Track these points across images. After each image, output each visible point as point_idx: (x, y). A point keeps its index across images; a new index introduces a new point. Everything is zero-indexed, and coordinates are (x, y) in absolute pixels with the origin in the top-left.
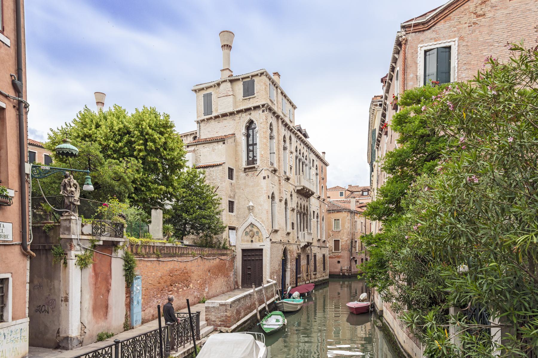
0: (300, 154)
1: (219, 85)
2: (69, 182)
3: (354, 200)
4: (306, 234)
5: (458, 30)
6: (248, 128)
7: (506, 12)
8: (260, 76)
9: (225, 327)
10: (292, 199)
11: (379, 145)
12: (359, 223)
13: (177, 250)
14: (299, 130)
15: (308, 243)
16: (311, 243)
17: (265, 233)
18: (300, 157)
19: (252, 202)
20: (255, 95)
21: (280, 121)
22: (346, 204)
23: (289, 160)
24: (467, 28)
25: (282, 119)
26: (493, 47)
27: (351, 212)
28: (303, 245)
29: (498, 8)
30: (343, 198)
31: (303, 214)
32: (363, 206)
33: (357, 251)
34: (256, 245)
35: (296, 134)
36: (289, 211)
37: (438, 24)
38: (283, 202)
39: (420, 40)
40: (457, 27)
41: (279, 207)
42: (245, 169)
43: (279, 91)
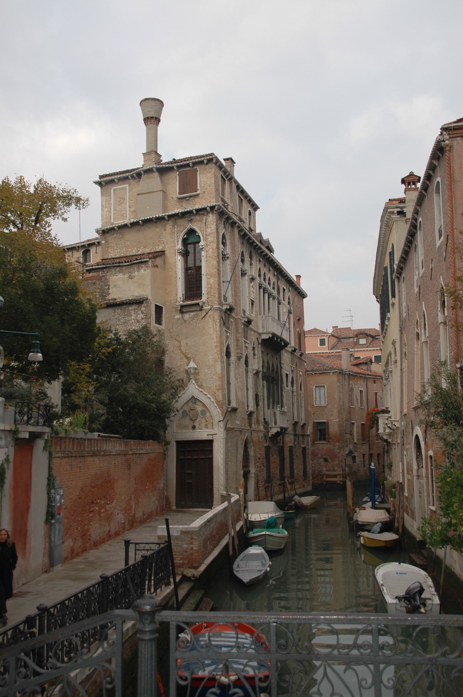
0: (265, 279)
1: (139, 175)
4: (278, 413)
8: (207, 164)
11: (400, 274)
12: (356, 392)
15: (282, 428)
16: (286, 429)
17: (216, 413)
18: (266, 284)
19: (194, 361)
20: (199, 192)
21: (236, 230)
23: (249, 290)
27: (341, 373)
28: (273, 431)
30: (325, 350)
31: (272, 378)
32: (361, 364)
33: (355, 441)
34: (202, 434)
35: (260, 248)
36: (250, 375)
41: (236, 371)
42: (182, 306)
43: (234, 186)
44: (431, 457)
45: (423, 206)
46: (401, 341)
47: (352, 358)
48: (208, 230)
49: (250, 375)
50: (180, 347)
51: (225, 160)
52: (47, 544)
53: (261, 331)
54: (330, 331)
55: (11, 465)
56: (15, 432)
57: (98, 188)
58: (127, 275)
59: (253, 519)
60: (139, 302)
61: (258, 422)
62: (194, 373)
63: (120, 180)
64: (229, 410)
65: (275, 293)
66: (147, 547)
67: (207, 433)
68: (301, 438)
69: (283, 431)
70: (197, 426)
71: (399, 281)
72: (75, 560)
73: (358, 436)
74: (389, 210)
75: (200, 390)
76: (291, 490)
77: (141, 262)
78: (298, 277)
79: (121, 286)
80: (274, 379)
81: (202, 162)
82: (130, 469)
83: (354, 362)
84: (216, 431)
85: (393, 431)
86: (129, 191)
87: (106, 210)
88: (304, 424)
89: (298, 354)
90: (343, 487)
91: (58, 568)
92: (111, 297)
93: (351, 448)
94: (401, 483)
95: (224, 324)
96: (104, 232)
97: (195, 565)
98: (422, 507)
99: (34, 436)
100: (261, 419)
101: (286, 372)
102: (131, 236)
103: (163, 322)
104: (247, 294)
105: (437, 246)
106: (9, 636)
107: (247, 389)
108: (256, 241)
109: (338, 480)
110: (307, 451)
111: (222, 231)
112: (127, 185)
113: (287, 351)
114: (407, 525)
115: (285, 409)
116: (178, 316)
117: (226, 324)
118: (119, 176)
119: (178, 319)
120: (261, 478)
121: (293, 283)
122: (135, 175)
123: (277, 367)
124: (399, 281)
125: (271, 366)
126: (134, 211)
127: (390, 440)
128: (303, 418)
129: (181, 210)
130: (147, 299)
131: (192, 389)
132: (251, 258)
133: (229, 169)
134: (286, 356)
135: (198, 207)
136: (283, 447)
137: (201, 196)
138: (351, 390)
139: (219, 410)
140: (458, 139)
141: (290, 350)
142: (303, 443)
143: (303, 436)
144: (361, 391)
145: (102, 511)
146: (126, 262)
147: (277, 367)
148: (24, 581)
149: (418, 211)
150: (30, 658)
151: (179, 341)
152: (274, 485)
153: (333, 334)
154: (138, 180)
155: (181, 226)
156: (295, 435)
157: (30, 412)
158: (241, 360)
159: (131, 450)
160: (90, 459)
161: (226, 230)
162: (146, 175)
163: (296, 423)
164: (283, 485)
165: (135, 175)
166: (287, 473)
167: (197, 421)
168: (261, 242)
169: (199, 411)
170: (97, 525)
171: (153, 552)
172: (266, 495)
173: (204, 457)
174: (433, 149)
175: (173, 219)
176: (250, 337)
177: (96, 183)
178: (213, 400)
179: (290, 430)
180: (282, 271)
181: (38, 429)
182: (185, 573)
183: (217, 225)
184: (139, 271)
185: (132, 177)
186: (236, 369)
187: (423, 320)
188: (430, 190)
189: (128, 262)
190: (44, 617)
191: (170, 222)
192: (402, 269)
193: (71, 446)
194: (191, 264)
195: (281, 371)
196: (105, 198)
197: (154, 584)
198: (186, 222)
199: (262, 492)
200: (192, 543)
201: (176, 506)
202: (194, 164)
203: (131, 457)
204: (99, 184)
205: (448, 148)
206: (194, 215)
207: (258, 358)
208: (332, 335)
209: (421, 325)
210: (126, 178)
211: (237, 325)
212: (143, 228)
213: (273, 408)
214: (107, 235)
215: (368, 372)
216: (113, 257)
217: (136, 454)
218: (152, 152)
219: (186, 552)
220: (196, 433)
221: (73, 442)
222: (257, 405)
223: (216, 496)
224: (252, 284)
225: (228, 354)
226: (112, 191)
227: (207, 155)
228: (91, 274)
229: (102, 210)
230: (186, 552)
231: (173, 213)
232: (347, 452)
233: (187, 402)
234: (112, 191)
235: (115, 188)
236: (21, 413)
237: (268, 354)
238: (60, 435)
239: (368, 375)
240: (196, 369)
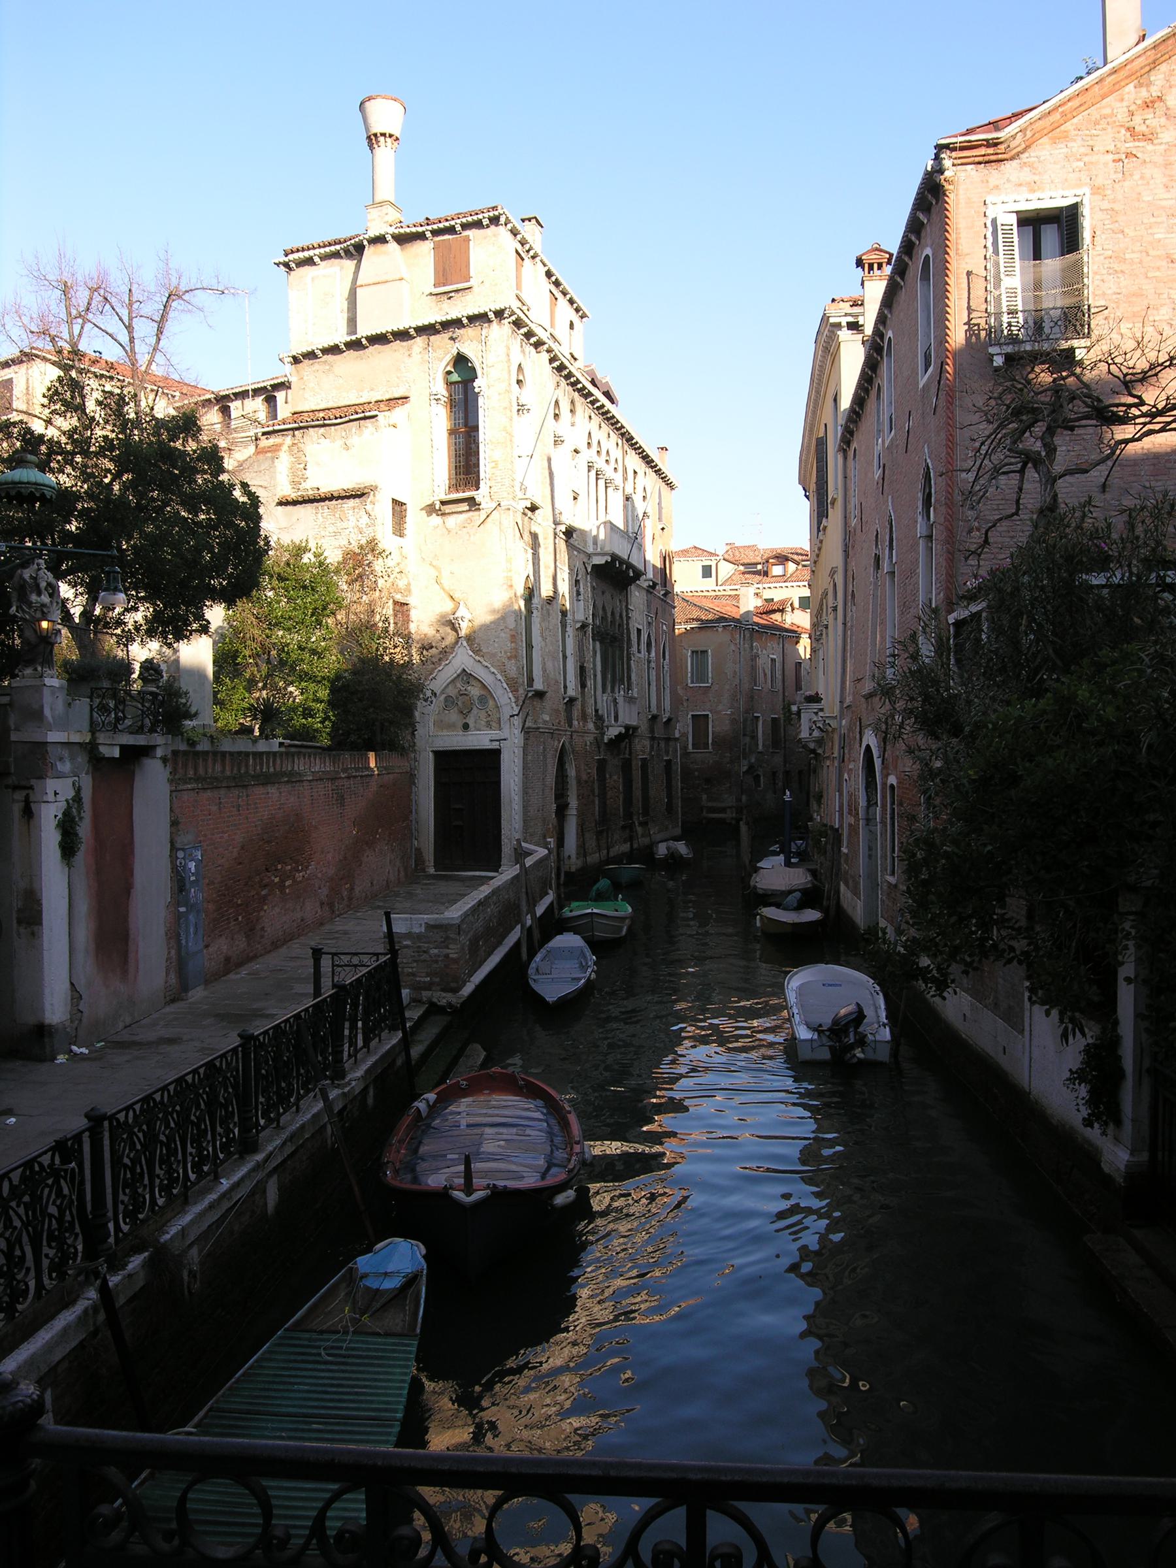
2: (35, 579)
4: (620, 700)
9: (443, 990)
13: (278, 761)
15: (627, 728)
16: (635, 728)
17: (506, 700)
18: (600, 463)
21: (545, 357)
24: (1112, 165)
28: (613, 732)
34: (479, 739)
35: (590, 394)
36: (570, 631)
40: (1086, 159)
44: (892, 786)
46: (846, 571)
52: (173, 952)
53: (590, 550)
54: (721, 550)
55: (87, 814)
56: (91, 749)
61: (584, 717)
63: (324, 258)
65: (618, 478)
67: (489, 737)
69: (629, 733)
70: (471, 725)
72: (232, 976)
73: (764, 741)
76: (643, 836)
80: (614, 639)
81: (478, 224)
84: (505, 733)
85: (826, 730)
88: (669, 720)
90: (737, 830)
91: (197, 994)
93: (753, 760)
94: (837, 830)
97: (453, 985)
98: (873, 888)
99: (134, 755)
100: (590, 710)
105: (921, 386)
106: (16, 1182)
107: (565, 657)
109: (729, 815)
110: (674, 768)
114: (845, 904)
115: (635, 692)
122: (351, 248)
125: (609, 615)
127: (820, 751)
128: (668, 708)
134: (637, 597)
138: (754, 658)
139: (511, 695)
141: (645, 585)
142: (667, 753)
143: (668, 740)
144: (773, 660)
145: (287, 883)
147: (621, 616)
148: (128, 1020)
149: (886, 317)
150: (493, 878)
153: (726, 556)
156: (653, 738)
157: (121, 707)
159: (345, 770)
160: (260, 790)
163: (654, 718)
164: (630, 827)
165: (351, 248)
167: (471, 715)
168: (593, 382)
169: (476, 698)
170: (277, 910)
171: (365, 970)
174: (920, 188)
178: (499, 677)
179: (644, 729)
181: (141, 740)
182: (435, 1000)
186: (543, 620)
187: (888, 530)
188: (910, 274)
190: (102, 1133)
193: (218, 767)
195: (628, 624)
197: (363, 1029)
203: (346, 783)
209: (883, 542)
213: (613, 691)
217: (355, 777)
221: (223, 761)
222: (583, 685)
223: (507, 849)
230: (437, 962)
232: (745, 769)
236: (104, 709)
238: (199, 748)
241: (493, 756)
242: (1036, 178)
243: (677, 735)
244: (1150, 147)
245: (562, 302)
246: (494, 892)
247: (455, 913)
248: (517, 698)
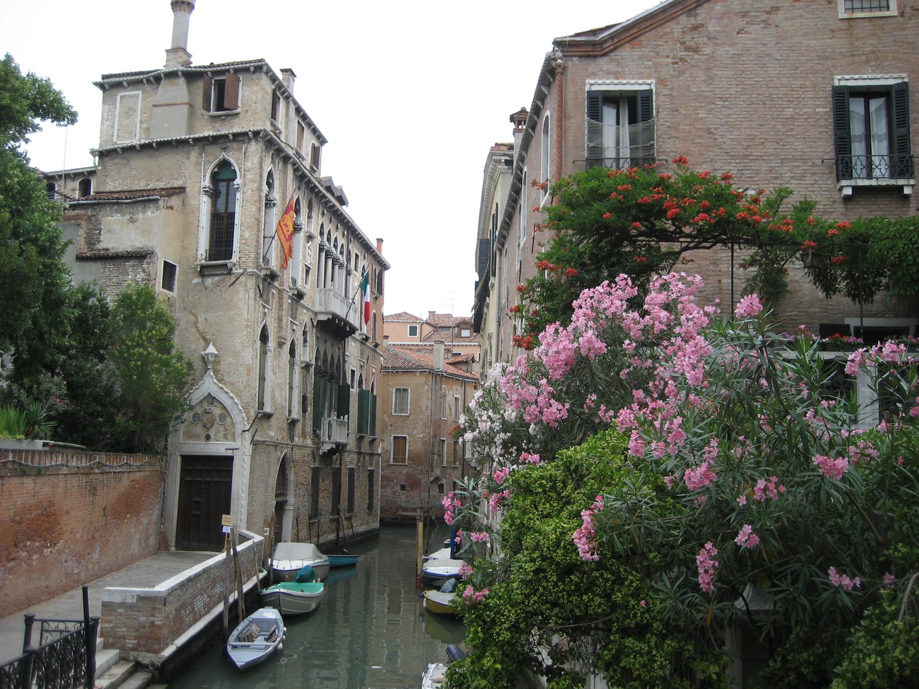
0: (329, 240)
3: (442, 347)
5: (656, 65)
6: (215, 178)
7: (732, 50)
8: (254, 72)
9: (148, 651)
10: (305, 341)
11: (503, 245)
12: (450, 399)
13: (37, 458)
14: (329, 189)
15: (338, 444)
16: (344, 445)
17: (241, 420)
19: (214, 345)
20: (239, 110)
21: (290, 169)
22: (422, 354)
23: (304, 253)
24: (671, 65)
25: (294, 164)
26: (714, 106)
28: (326, 447)
29: (719, 42)
30: (415, 341)
33: (445, 464)
34: (218, 448)
35: (324, 196)
36: (297, 369)
37: (621, 49)
38: (287, 348)
39: (589, 72)
41: (277, 363)
42: (203, 267)
43: (292, 108)
45: (530, 150)
47: (450, 355)
48: (250, 164)
49: (297, 369)
50: (195, 324)
51: (282, 71)
53: (317, 309)
57: (99, 93)
58: (127, 217)
59: (280, 568)
60: (140, 256)
61: (304, 435)
62: (214, 361)
64: (260, 415)
66: (62, 626)
67: (226, 447)
68: (367, 458)
71: (501, 255)
74: (494, 158)
75: (221, 385)
77: (149, 201)
78: (380, 241)
79: (119, 232)
80: (332, 377)
82: (94, 494)
83: (452, 360)
86: (143, 99)
87: (108, 123)
89: (370, 344)
92: (101, 246)
95: (261, 296)
96: (103, 154)
101: (352, 368)
102: (139, 163)
103: (176, 287)
104: (301, 258)
107: (291, 388)
108: (318, 185)
110: (375, 476)
111: (268, 167)
112: (140, 92)
113: (354, 338)
116: (197, 280)
117: (265, 297)
118: (129, 78)
119: (197, 284)
120: (303, 510)
121: (371, 248)
123: (339, 360)
124: (501, 255)
125: (329, 358)
126: (148, 129)
129: (212, 133)
130: (152, 253)
131: (209, 385)
132: (310, 208)
133: (285, 84)
134: (352, 347)
135: (236, 130)
136: (340, 469)
137: (241, 116)
139: (244, 415)
140: (575, 59)
141: (359, 338)
142: (371, 464)
143: (372, 455)
146: (127, 199)
147: (339, 360)
151: (195, 316)
152: (323, 520)
153: (429, 321)
154: (156, 86)
155: (211, 154)
156: (359, 453)
158: (284, 347)
160: (16, 481)
161: (274, 165)
162: (167, 81)
166: (344, 503)
170: (23, 579)
172: (310, 534)
173: (218, 480)
175: (201, 144)
176: (300, 317)
177: (96, 84)
180: (355, 230)
182: (140, 659)
183: (261, 158)
184: (144, 213)
185: (148, 81)
186: (275, 359)
189: (130, 198)
191: (196, 148)
192: (505, 237)
194: (221, 208)
195: (344, 366)
196: (107, 106)
198: (219, 150)
199: (304, 533)
200: (153, 616)
201: (176, 546)
202: (237, 71)
203: (100, 477)
204: (101, 86)
205: (559, 70)
206: (230, 141)
207: (311, 347)
208: (427, 323)
210: (140, 82)
211: (281, 298)
212: (157, 153)
214: (106, 159)
215: (468, 375)
216: (112, 190)
218: (178, 49)
219: (144, 627)
220: (211, 446)
224: (309, 245)
225: (264, 338)
226: (118, 98)
227: (255, 61)
228: (76, 212)
229: (102, 124)
230: (144, 627)
231: (201, 135)
232: (432, 479)
233: (201, 402)
234: (118, 98)
235: (123, 94)
237: (325, 342)
239: (468, 378)
240: (216, 355)
241: (226, 462)
242: (620, 70)
243: (380, 452)
244: (696, 56)
245: (307, 132)
246: (205, 571)
247: (164, 586)
248: (248, 418)
